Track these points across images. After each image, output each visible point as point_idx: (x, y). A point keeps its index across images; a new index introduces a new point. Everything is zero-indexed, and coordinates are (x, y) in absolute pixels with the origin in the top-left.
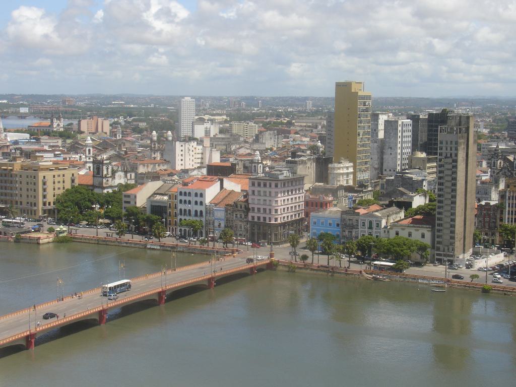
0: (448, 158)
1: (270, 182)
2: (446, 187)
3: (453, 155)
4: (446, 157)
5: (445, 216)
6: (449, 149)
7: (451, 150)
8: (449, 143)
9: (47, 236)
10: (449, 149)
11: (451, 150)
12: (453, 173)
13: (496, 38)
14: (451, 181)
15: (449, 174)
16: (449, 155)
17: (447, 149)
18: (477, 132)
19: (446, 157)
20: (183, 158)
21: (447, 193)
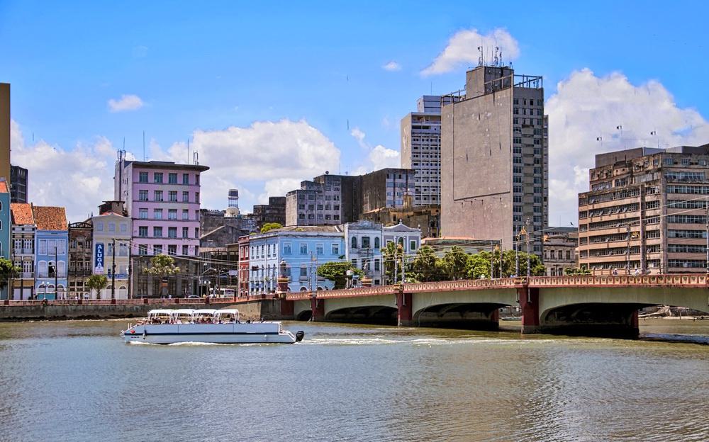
0: (528, 126)
1: (186, 172)
2: (526, 174)
3: (535, 122)
4: (524, 126)
5: (525, 174)
6: (528, 111)
7: (532, 113)
8: (528, 102)
9: (702, 318)
10: (528, 111)
11: (532, 113)
12: (535, 152)
13: (117, 106)
14: (533, 136)
15: (529, 153)
16: (528, 123)
17: (525, 102)
18: (526, 287)
19: (524, 126)
20: (255, 258)
21: (528, 184)
